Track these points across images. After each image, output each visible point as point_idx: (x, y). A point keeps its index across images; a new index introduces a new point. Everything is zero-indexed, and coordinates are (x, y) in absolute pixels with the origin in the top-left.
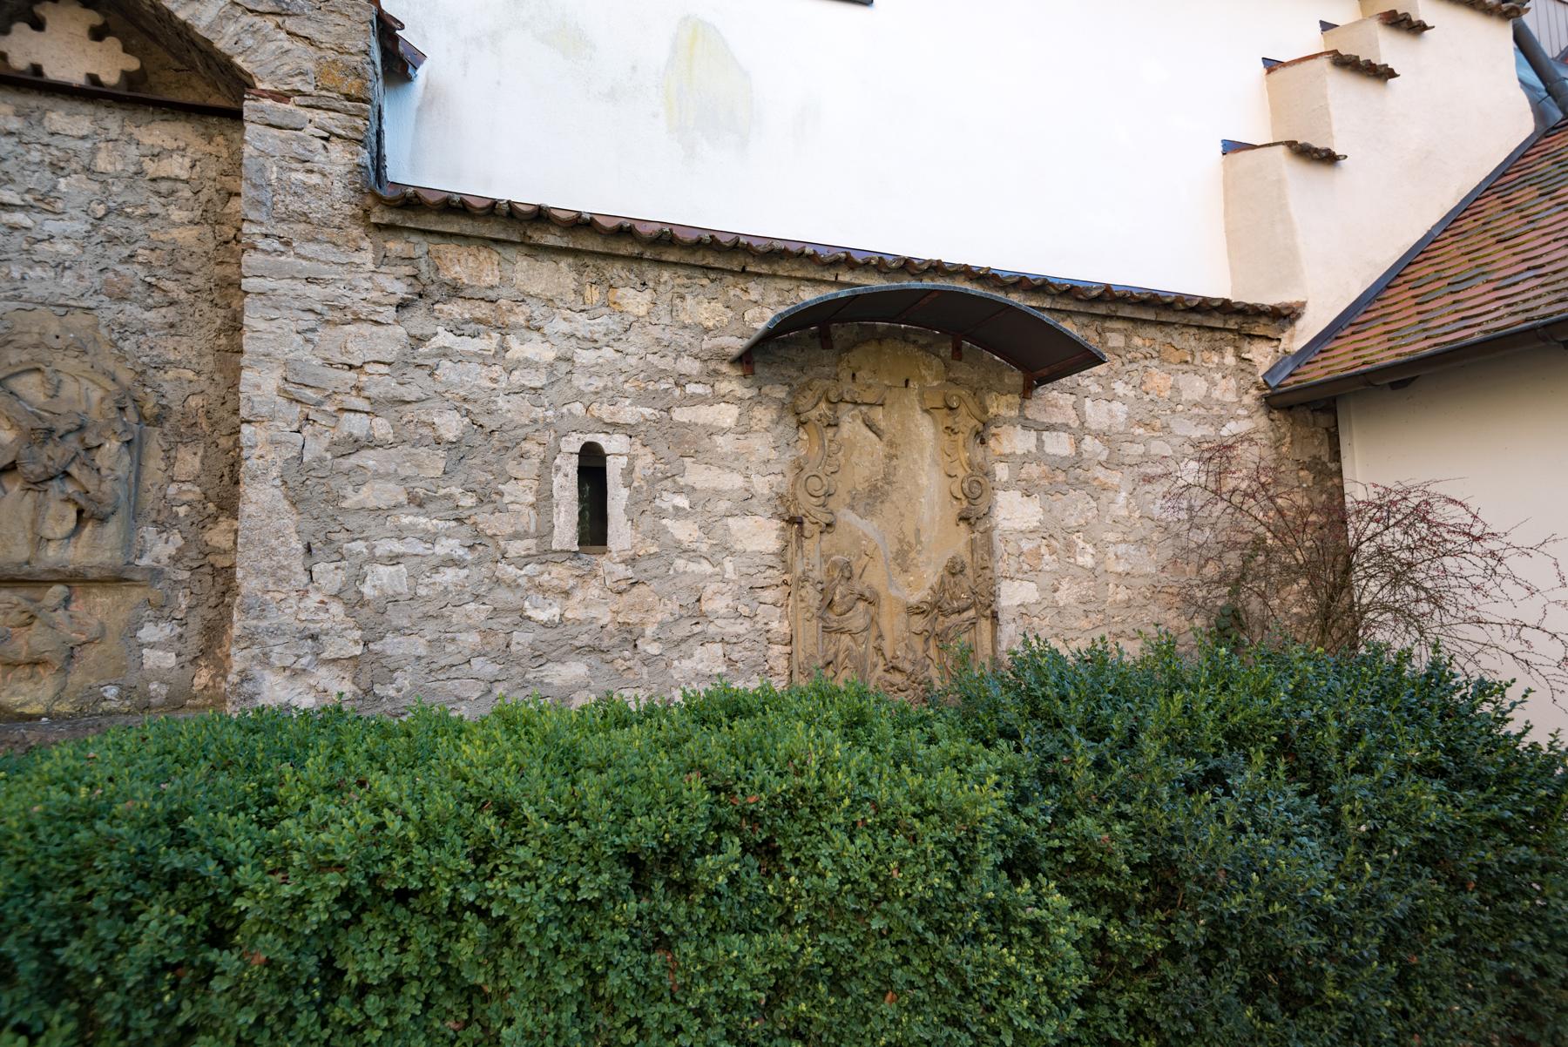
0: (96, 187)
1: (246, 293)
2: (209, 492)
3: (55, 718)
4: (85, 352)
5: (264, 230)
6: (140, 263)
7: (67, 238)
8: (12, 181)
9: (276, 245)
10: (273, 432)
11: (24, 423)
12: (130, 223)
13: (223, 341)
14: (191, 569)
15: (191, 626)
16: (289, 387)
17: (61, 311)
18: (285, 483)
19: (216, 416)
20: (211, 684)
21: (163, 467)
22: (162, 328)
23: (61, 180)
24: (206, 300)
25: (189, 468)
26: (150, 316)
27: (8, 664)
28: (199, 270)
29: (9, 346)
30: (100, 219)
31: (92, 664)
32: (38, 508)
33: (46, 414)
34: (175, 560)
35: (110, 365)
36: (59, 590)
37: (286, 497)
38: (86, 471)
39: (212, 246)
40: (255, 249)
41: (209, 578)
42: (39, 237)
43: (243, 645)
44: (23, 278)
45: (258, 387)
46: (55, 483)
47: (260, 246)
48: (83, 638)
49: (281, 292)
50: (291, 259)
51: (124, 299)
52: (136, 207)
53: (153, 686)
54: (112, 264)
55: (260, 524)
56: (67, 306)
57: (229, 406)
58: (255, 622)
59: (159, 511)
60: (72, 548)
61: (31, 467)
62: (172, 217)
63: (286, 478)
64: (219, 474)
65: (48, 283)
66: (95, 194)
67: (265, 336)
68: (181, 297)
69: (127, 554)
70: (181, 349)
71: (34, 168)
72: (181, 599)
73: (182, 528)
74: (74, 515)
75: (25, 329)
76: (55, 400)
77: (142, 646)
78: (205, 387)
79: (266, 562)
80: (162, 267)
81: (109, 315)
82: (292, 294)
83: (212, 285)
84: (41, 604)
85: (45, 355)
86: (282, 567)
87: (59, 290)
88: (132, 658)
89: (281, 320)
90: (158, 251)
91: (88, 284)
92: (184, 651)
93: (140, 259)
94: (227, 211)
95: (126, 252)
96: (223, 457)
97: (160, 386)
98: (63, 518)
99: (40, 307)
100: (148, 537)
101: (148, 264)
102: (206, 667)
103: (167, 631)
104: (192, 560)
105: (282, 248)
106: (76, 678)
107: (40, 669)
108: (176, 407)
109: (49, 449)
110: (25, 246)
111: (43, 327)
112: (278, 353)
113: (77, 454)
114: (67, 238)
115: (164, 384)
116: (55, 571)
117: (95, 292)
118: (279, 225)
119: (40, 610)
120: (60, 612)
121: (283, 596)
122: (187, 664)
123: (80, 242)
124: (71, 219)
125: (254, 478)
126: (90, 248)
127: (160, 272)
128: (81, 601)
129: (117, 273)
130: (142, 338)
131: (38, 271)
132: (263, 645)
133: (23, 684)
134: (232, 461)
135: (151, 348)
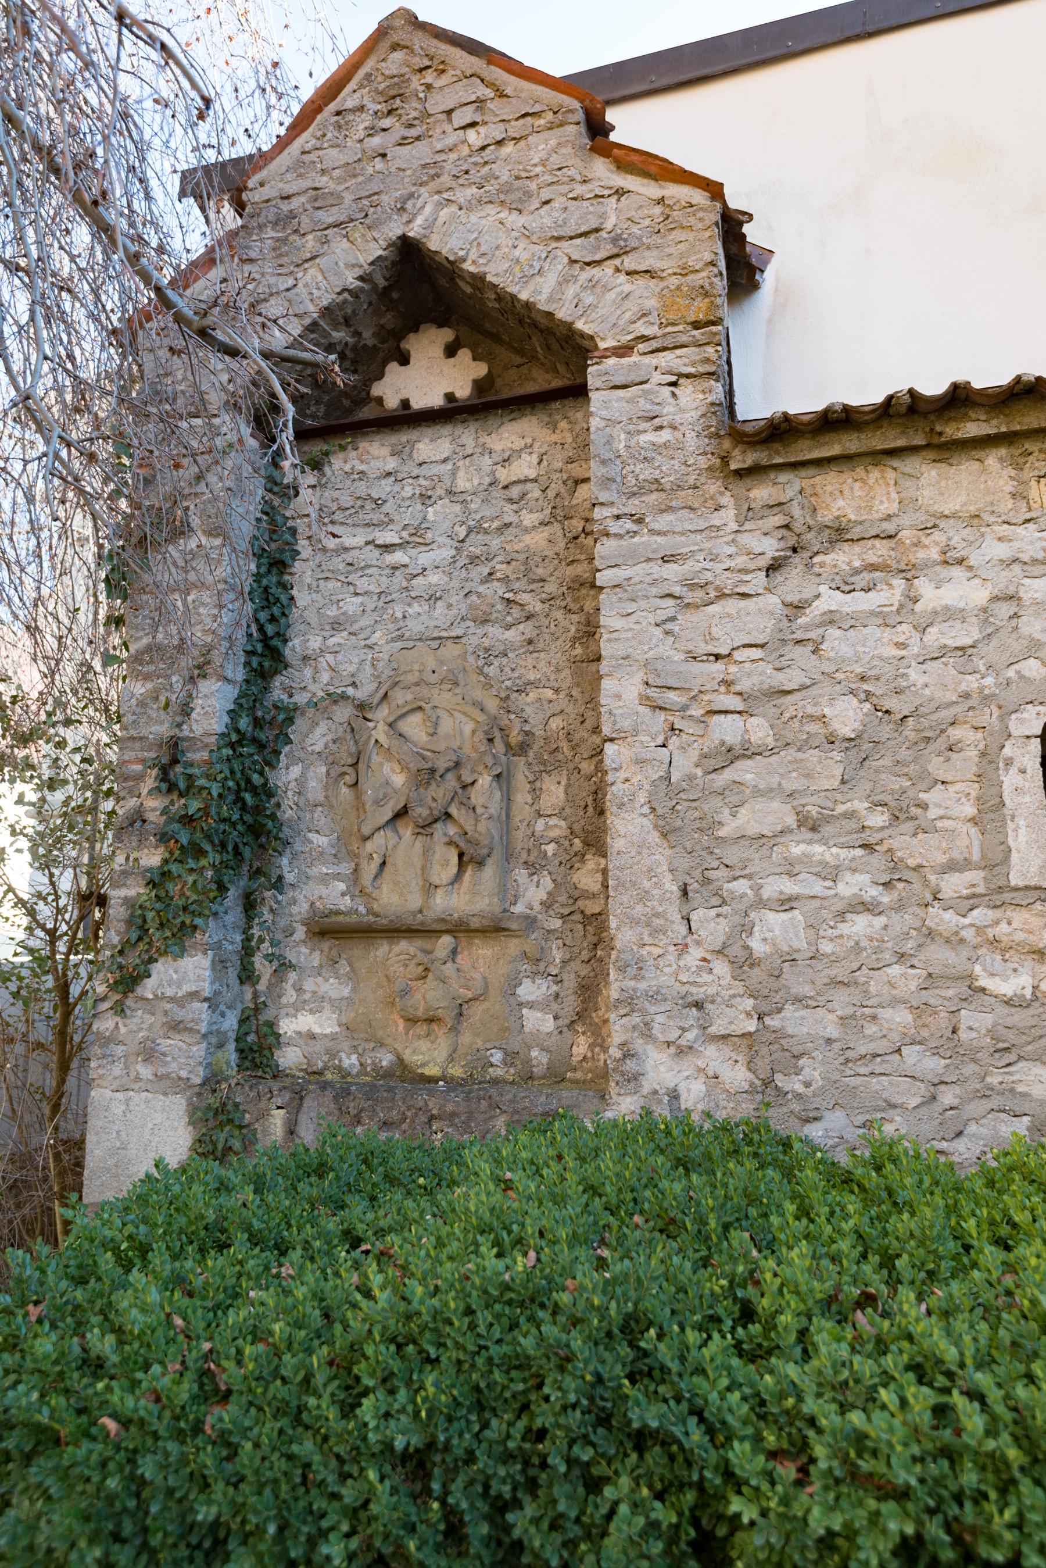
0: (457, 508)
4: (457, 684)
5: (616, 512)
8: (392, 521)
9: (630, 525)
13: (578, 651)
14: (563, 917)
15: (566, 983)
16: (651, 692)
17: (435, 644)
18: (653, 810)
19: (577, 737)
25: (554, 800)
26: (510, 635)
32: (427, 852)
34: (547, 905)
35: (478, 694)
36: (446, 940)
39: (562, 545)
40: (607, 535)
43: (622, 1012)
45: (618, 697)
46: (439, 826)
47: (613, 530)
48: (470, 995)
49: (636, 579)
50: (646, 538)
53: (535, 1053)
57: (589, 724)
58: (633, 983)
61: (419, 810)
63: (655, 805)
65: (424, 618)
67: (623, 635)
69: (502, 900)
77: (521, 1004)
79: (639, 909)
81: (474, 641)
82: (648, 579)
85: (425, 692)
86: (657, 915)
87: (433, 623)
91: (455, 611)
92: (561, 1013)
93: (499, 575)
94: (575, 502)
95: (486, 571)
98: (447, 863)
100: (521, 881)
101: (505, 580)
105: (635, 528)
106: (466, 1038)
107: (435, 1026)
108: (539, 732)
110: (405, 584)
112: (638, 655)
116: (443, 920)
119: (433, 961)
121: (661, 951)
125: (621, 806)
127: (516, 586)
130: (505, 660)
131: (416, 608)
132: (643, 1012)
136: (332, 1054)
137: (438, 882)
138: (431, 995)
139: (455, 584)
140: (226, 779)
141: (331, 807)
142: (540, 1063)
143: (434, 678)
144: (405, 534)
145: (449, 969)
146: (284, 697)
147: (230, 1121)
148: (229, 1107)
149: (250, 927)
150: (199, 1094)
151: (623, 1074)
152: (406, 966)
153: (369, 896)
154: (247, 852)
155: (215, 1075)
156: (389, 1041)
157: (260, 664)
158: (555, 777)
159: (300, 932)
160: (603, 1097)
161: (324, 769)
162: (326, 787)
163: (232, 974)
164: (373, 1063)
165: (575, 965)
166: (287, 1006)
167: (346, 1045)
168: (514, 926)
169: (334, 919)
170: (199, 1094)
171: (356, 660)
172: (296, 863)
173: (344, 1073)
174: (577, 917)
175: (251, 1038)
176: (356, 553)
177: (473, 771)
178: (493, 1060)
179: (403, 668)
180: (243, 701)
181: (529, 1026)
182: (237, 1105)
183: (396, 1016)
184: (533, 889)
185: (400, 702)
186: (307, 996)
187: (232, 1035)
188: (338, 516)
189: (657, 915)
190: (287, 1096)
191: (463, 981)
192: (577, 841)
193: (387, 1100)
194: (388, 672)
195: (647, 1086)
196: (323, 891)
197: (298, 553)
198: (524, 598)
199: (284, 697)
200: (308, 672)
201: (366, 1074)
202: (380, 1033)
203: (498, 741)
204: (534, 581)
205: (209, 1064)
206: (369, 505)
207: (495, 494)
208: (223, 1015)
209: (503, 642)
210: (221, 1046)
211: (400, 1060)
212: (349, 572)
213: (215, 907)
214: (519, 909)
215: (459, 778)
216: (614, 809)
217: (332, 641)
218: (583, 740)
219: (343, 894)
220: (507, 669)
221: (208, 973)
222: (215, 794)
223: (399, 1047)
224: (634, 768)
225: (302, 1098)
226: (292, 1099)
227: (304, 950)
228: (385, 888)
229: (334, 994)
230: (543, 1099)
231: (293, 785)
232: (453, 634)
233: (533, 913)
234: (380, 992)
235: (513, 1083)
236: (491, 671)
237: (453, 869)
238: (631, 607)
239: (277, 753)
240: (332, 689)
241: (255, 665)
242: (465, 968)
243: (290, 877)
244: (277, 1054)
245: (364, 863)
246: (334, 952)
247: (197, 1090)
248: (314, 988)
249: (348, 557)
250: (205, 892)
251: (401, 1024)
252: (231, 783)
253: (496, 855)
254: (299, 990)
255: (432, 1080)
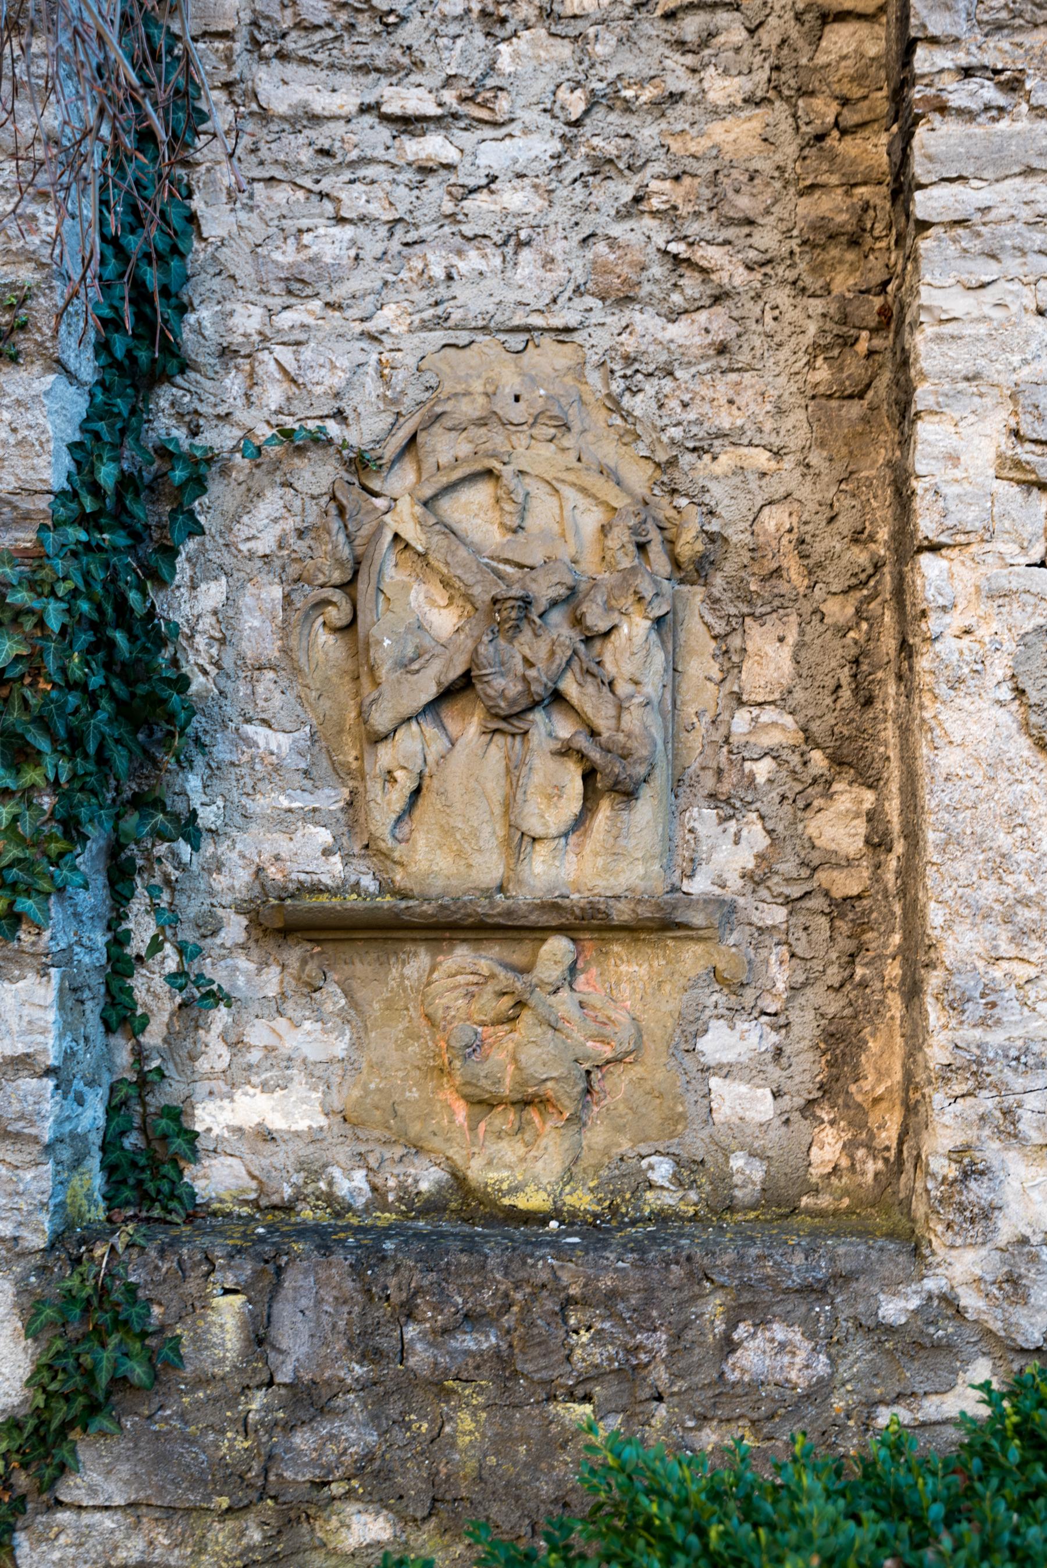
0: (565, 50)
1: (924, 226)
2: (814, 726)
3: (570, 1219)
4: (567, 427)
5: (963, 60)
6: (654, 214)
7: (520, 176)
8: (419, 65)
9: (990, 93)
10: (992, 568)
11: (477, 590)
12: (629, 123)
13: (822, 374)
14: (788, 901)
15: (796, 1030)
16: (1026, 453)
17: (516, 341)
18: (1020, 692)
19: (818, 549)
20: (844, 1163)
21: (717, 676)
22: (704, 357)
23: (502, 47)
24: (783, 282)
25: (770, 673)
26: (679, 331)
27: (480, 1102)
28: (767, 212)
29: (437, 429)
30: (577, 124)
31: (621, 1107)
32: (513, 771)
33: (509, 569)
34: (755, 880)
35: (609, 452)
36: (558, 946)
37: (1026, 726)
38: (591, 689)
39: (791, 150)
40: (943, 109)
41: (823, 921)
42: (472, 182)
43: (958, 1089)
44: (450, 277)
45: (953, 459)
46: (538, 716)
47: (955, 100)
48: (607, 1052)
49: (1002, 212)
50: (1022, 125)
51: (629, 299)
52: (641, 83)
53: (738, 1162)
54: (602, 222)
55: (972, 794)
56: (528, 329)
57: (845, 524)
58: (978, 1033)
59: (719, 772)
60: (571, 857)
61: (499, 683)
62: (711, 96)
63: (1025, 683)
64: (831, 683)
65: (491, 283)
66: (563, 68)
67: (969, 330)
68: (737, 281)
69: (667, 868)
70: (740, 401)
71: (454, 29)
72: (774, 969)
73: (764, 810)
74: (577, 785)
75: (460, 388)
76: (521, 536)
77: (705, 1069)
78: (792, 485)
79: (989, 889)
80: (697, 214)
81: (602, 339)
82: (1026, 214)
83: (794, 244)
84: (533, 978)
85: (497, 439)
86: (1025, 902)
87: (512, 296)
88: (692, 1097)
89: (1002, 285)
90: (687, 181)
91: (561, 274)
92: (787, 1086)
93: (656, 203)
94: (821, 59)
95: (628, 193)
96: (837, 643)
97: (704, 490)
98: (559, 791)
99: (480, 337)
100: (702, 831)
101: (669, 215)
102: (832, 1123)
103: (753, 1040)
104: (788, 880)
105: (1000, 99)
106: (597, 1136)
107: (533, 1114)
108: (737, 536)
109: (526, 644)
110: (448, 207)
111: (489, 381)
112: (994, 371)
113: (575, 652)
114: (520, 176)
115: (711, 485)
116: (555, 907)
117: (577, 290)
118: (992, 42)
119: (532, 988)
120: (564, 994)
121: (1032, 972)
122: (796, 1116)
123: (543, 181)
124: (526, 131)
125: (956, 683)
126: (562, 193)
127: (693, 229)
128: (594, 971)
129: (612, 242)
130: (668, 384)
131: (472, 261)
132: (1000, 1089)
133: (504, 1144)
134: (854, 651)
135: (685, 405)
136: (313, 1171)
137: (538, 830)
138: (530, 1056)
139: (560, 214)
140: (75, 593)
141: (297, 671)
142: (748, 1181)
143: (517, 413)
144: (449, 96)
145: (564, 1003)
146: (180, 433)
147: (121, 1324)
148: (117, 1296)
149: (122, 917)
150: (42, 1270)
151: (961, 1208)
152: (471, 996)
153: (386, 856)
154: (120, 759)
155: (70, 1226)
156: (437, 1143)
157: (129, 353)
158: (772, 627)
159: (235, 928)
160: (916, 1252)
161: (277, 592)
162: (285, 630)
163: (93, 1010)
164: (402, 1186)
165: (817, 995)
166: (210, 1076)
167: (342, 1153)
168: (698, 919)
169: (311, 902)
170: (42, 1270)
171: (343, 362)
172: (218, 786)
173: (339, 1208)
174: (817, 903)
175: (132, 1140)
176: (338, 129)
177: (609, 608)
178: (655, 1177)
179: (448, 388)
180: (101, 426)
181: (723, 1112)
182: (131, 1290)
183: (447, 1095)
184: (727, 846)
185: (444, 459)
186: (254, 1056)
187: (96, 1139)
188: (295, 43)
189: (1025, 902)
190: (248, 1268)
191: (593, 1028)
192: (817, 756)
193: (468, 1269)
194: (415, 393)
195: (1006, 1230)
196: (281, 843)
197: (204, 117)
198: (710, 255)
199: (180, 433)
200: (234, 383)
201: (385, 1207)
202: (415, 1129)
203: (656, 551)
204: (731, 222)
205: (61, 1205)
206: (366, 26)
207: (646, 28)
208: (80, 1100)
209: (666, 346)
210: (77, 1163)
211: (459, 1180)
212: (323, 171)
213: (62, 874)
214: (699, 886)
215: (578, 621)
216: (943, 689)
217: (285, 320)
218: (831, 556)
219: (327, 852)
220: (674, 404)
221: (52, 1015)
222: (54, 624)
223: (457, 1154)
224: (986, 607)
225: (279, 1271)
226: (258, 1275)
227: (244, 964)
228: (421, 841)
229: (313, 1053)
230: (799, 1259)
231: (207, 622)
232: (557, 322)
233: (727, 895)
234: (414, 1048)
235: (695, 1218)
236: (639, 405)
237: (572, 804)
238: (987, 271)
239: (171, 552)
240: (290, 423)
241: (119, 353)
242: (596, 998)
243: (207, 817)
244: (190, 1171)
245: (375, 788)
246: (312, 968)
247: (37, 1260)
248: (271, 1040)
249: (322, 136)
250: (37, 842)
251: (461, 1112)
252: (84, 606)
253: (661, 779)
254: (237, 1045)
255: (539, 1218)
